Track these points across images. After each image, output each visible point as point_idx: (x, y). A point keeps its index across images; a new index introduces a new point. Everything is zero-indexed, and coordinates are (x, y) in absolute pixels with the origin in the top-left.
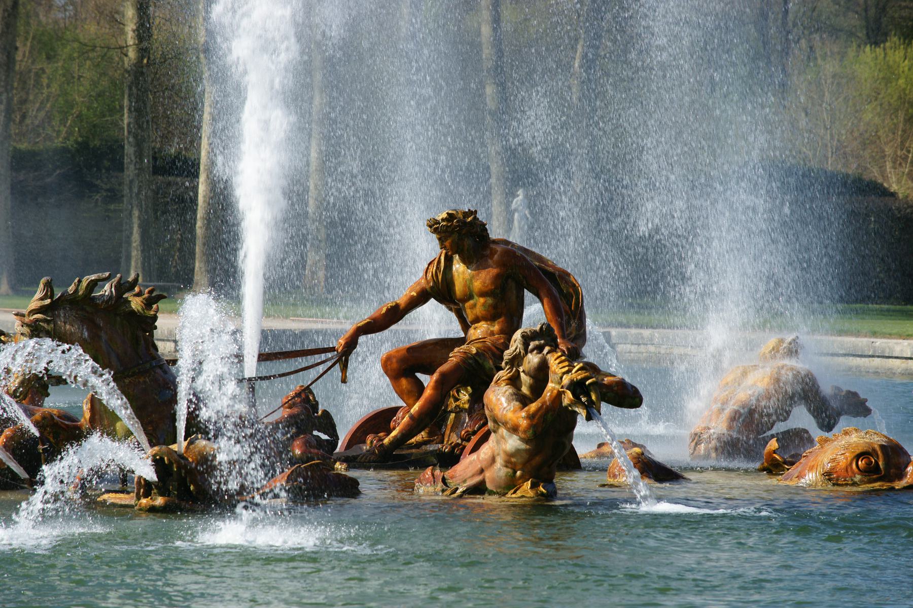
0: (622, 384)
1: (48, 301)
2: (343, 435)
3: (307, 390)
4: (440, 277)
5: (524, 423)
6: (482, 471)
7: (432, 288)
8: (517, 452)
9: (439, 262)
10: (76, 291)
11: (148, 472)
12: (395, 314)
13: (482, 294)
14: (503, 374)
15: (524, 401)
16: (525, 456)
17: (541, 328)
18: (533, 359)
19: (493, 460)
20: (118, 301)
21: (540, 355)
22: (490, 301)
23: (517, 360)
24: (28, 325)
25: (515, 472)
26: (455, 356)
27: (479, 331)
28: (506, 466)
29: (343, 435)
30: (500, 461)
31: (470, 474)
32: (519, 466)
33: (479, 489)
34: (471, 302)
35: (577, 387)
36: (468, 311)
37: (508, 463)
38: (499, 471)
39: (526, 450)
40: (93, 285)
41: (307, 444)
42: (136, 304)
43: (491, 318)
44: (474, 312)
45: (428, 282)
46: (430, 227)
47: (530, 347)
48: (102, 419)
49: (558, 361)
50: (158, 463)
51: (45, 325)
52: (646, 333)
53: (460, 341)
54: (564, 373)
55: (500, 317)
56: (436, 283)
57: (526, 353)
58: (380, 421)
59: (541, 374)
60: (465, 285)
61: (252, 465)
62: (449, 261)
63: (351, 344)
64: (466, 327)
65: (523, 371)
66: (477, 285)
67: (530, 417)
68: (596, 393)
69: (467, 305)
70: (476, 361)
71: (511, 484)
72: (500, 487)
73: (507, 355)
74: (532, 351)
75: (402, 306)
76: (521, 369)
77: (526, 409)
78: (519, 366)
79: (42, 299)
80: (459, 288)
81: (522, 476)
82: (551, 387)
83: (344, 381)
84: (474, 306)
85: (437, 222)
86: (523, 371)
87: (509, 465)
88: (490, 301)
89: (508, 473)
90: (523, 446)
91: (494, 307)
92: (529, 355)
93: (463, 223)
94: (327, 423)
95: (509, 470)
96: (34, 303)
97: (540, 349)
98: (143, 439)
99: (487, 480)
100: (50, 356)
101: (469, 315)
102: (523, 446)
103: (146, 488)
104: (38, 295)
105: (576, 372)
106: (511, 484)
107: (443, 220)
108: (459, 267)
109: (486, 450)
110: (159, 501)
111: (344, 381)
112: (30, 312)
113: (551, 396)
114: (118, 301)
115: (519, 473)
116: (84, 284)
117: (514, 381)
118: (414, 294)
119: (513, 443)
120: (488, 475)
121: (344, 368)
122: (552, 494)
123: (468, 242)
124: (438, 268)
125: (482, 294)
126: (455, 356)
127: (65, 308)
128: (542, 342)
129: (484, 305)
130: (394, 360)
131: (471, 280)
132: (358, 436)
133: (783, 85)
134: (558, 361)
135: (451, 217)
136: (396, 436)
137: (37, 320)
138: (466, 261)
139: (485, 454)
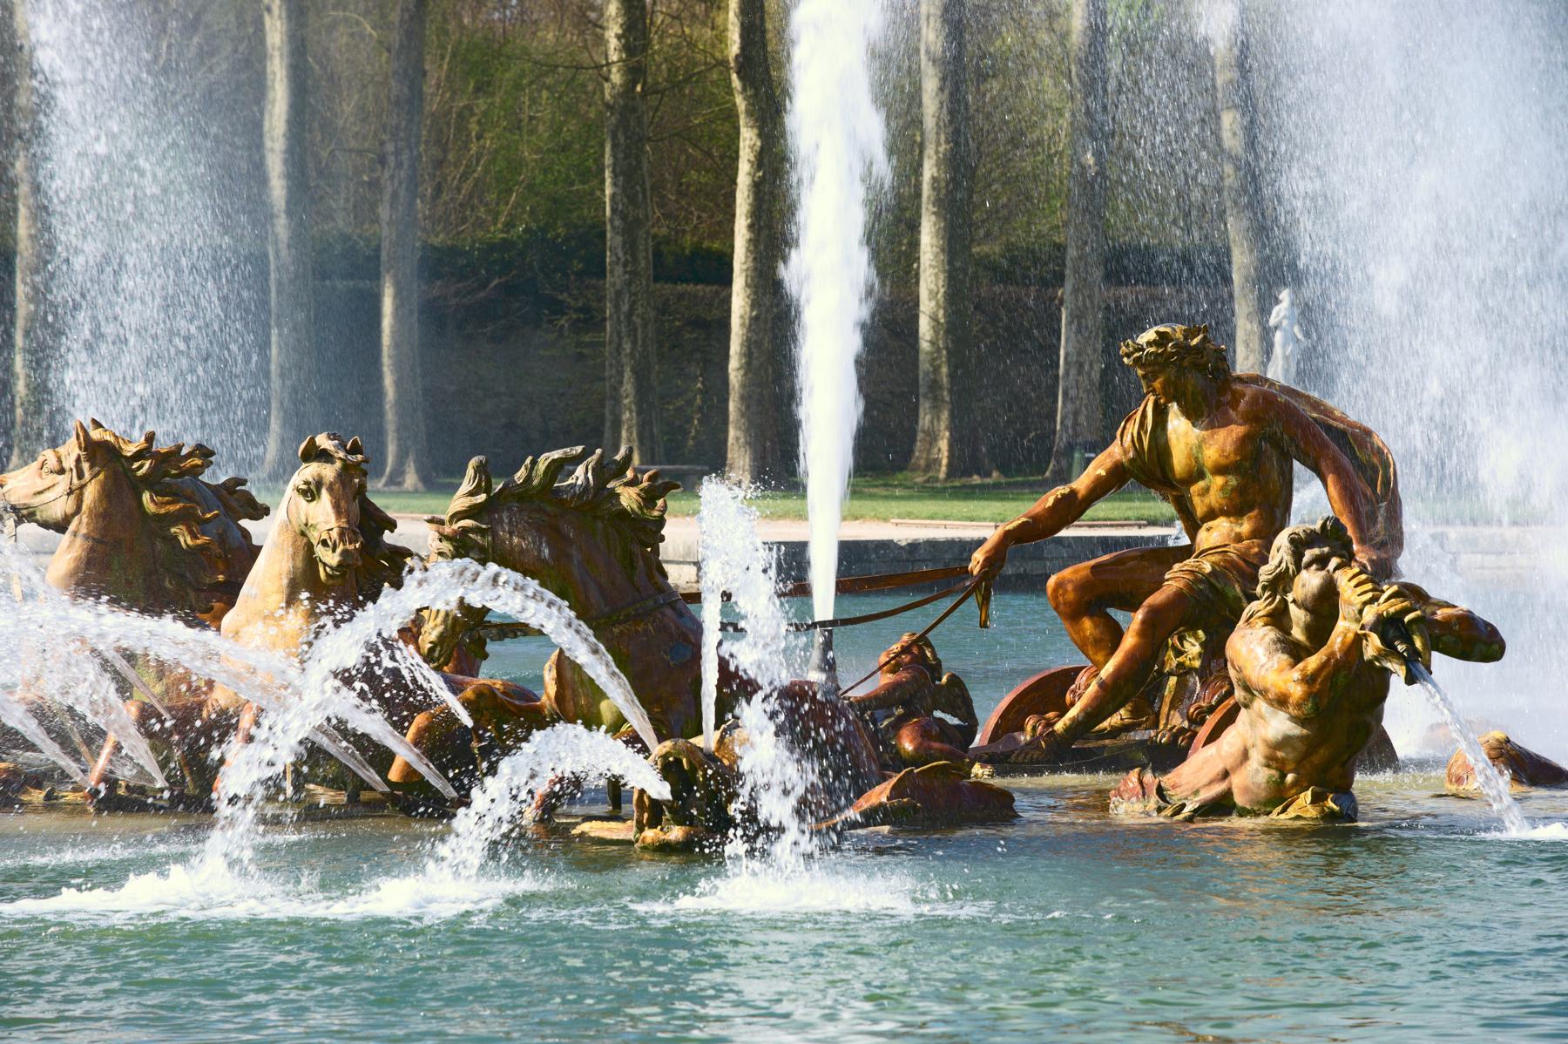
0: (1468, 620)
1: (482, 497)
2: (989, 710)
3: (922, 641)
5: (1297, 691)
6: (1226, 775)
7: (1131, 461)
8: (1285, 742)
10: (529, 478)
11: (646, 779)
13: (1220, 470)
14: (1259, 607)
15: (1296, 653)
17: (1324, 526)
18: (1309, 581)
20: (599, 494)
21: (1323, 573)
22: (1233, 481)
23: (1281, 582)
25: (1283, 776)
26: (1175, 579)
27: (1216, 533)
28: (1268, 766)
29: (989, 710)
30: (1257, 757)
31: (1206, 780)
32: (1291, 766)
33: (1221, 806)
34: (1201, 484)
35: (1389, 627)
36: (1196, 500)
37: (1270, 761)
38: (1253, 777)
39: (1301, 738)
40: (557, 468)
41: (924, 734)
42: (628, 498)
43: (1235, 510)
44: (1207, 501)
45: (1125, 452)
47: (1305, 559)
48: (577, 701)
50: (669, 769)
51: (478, 539)
53: (1186, 552)
54: (1365, 604)
55: (1251, 509)
56: (1139, 452)
57: (1299, 570)
58: (1050, 691)
59: (1325, 605)
60: (1190, 456)
62: (1161, 414)
64: (1193, 528)
66: (1211, 455)
67: (1308, 680)
68: (1422, 636)
69: (1194, 489)
70: (1212, 586)
71: (1278, 796)
72: (1258, 803)
73: (1265, 573)
74: (1308, 566)
76: (1290, 598)
77: (1300, 665)
78: (1286, 592)
79: (471, 494)
80: (1179, 461)
81: (1295, 784)
82: (1344, 628)
84: (1207, 490)
86: (1294, 601)
87: (1274, 764)
88: (1233, 481)
89: (1271, 777)
91: (1240, 490)
92: (1304, 572)
94: (958, 697)
95: (1273, 772)
96: (459, 502)
98: (638, 720)
99: (1235, 791)
100: (508, 595)
103: (654, 812)
104: (466, 486)
106: (1278, 796)
107: (1149, 344)
108: (1179, 427)
109: (1232, 739)
110: (676, 833)
112: (453, 517)
113: (1343, 643)
114: (599, 494)
115: (1290, 778)
116: (542, 466)
117: (1278, 619)
119: (1280, 725)
120: (1236, 781)
122: (1349, 812)
123: (1193, 381)
125: (1220, 470)
126: (1175, 579)
127: (510, 509)
128: (1326, 549)
129: (1222, 489)
131: (1200, 447)
132: (1011, 721)
134: (1355, 582)
137: (465, 530)
138: (1192, 414)
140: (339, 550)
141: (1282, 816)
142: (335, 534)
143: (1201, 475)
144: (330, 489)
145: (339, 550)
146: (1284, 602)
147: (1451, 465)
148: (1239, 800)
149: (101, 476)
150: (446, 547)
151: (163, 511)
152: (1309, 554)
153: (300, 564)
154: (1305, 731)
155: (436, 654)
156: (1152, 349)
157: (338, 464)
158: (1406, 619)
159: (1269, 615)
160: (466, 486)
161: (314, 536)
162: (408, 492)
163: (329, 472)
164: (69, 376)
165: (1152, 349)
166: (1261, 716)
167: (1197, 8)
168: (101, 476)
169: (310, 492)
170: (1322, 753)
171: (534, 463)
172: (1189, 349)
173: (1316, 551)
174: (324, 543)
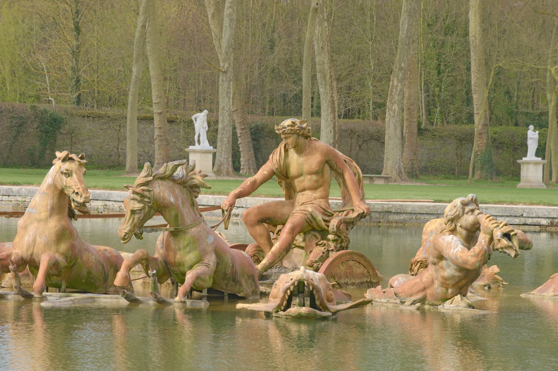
6: (424, 289)
7: (277, 169)
8: (453, 277)
16: (457, 280)
24: (137, 193)
25: (447, 290)
28: (442, 286)
30: (437, 284)
31: (416, 291)
39: (458, 277)
52: (15, 188)
54: (495, 227)
56: (280, 166)
57: (463, 215)
61: (501, 292)
65: (461, 226)
74: (467, 213)
75: (258, 181)
79: (146, 177)
80: (293, 170)
81: (452, 293)
82: (482, 238)
83: (226, 229)
85: (285, 128)
86: (461, 226)
87: (445, 286)
90: (457, 274)
92: (465, 216)
97: (472, 211)
99: (428, 295)
102: (457, 274)
105: (502, 227)
107: (288, 126)
108: (293, 155)
112: (138, 185)
113: (485, 241)
115: (450, 291)
120: (428, 291)
129: (310, 180)
130: (252, 215)
133: (293, 18)
134: (488, 220)
136: (265, 264)
137: (143, 190)
142: (81, 190)
143: (301, 175)
144: (76, 173)
146: (456, 225)
147: (65, 171)
150: (137, 197)
152: (467, 209)
153: (55, 201)
154: (460, 274)
155: (126, 237)
156: (290, 128)
158: (512, 234)
160: (143, 173)
161: (69, 192)
162: (532, 190)
164: (399, 142)
165: (290, 128)
166: (442, 268)
169: (68, 174)
170: (464, 282)
172: (302, 128)
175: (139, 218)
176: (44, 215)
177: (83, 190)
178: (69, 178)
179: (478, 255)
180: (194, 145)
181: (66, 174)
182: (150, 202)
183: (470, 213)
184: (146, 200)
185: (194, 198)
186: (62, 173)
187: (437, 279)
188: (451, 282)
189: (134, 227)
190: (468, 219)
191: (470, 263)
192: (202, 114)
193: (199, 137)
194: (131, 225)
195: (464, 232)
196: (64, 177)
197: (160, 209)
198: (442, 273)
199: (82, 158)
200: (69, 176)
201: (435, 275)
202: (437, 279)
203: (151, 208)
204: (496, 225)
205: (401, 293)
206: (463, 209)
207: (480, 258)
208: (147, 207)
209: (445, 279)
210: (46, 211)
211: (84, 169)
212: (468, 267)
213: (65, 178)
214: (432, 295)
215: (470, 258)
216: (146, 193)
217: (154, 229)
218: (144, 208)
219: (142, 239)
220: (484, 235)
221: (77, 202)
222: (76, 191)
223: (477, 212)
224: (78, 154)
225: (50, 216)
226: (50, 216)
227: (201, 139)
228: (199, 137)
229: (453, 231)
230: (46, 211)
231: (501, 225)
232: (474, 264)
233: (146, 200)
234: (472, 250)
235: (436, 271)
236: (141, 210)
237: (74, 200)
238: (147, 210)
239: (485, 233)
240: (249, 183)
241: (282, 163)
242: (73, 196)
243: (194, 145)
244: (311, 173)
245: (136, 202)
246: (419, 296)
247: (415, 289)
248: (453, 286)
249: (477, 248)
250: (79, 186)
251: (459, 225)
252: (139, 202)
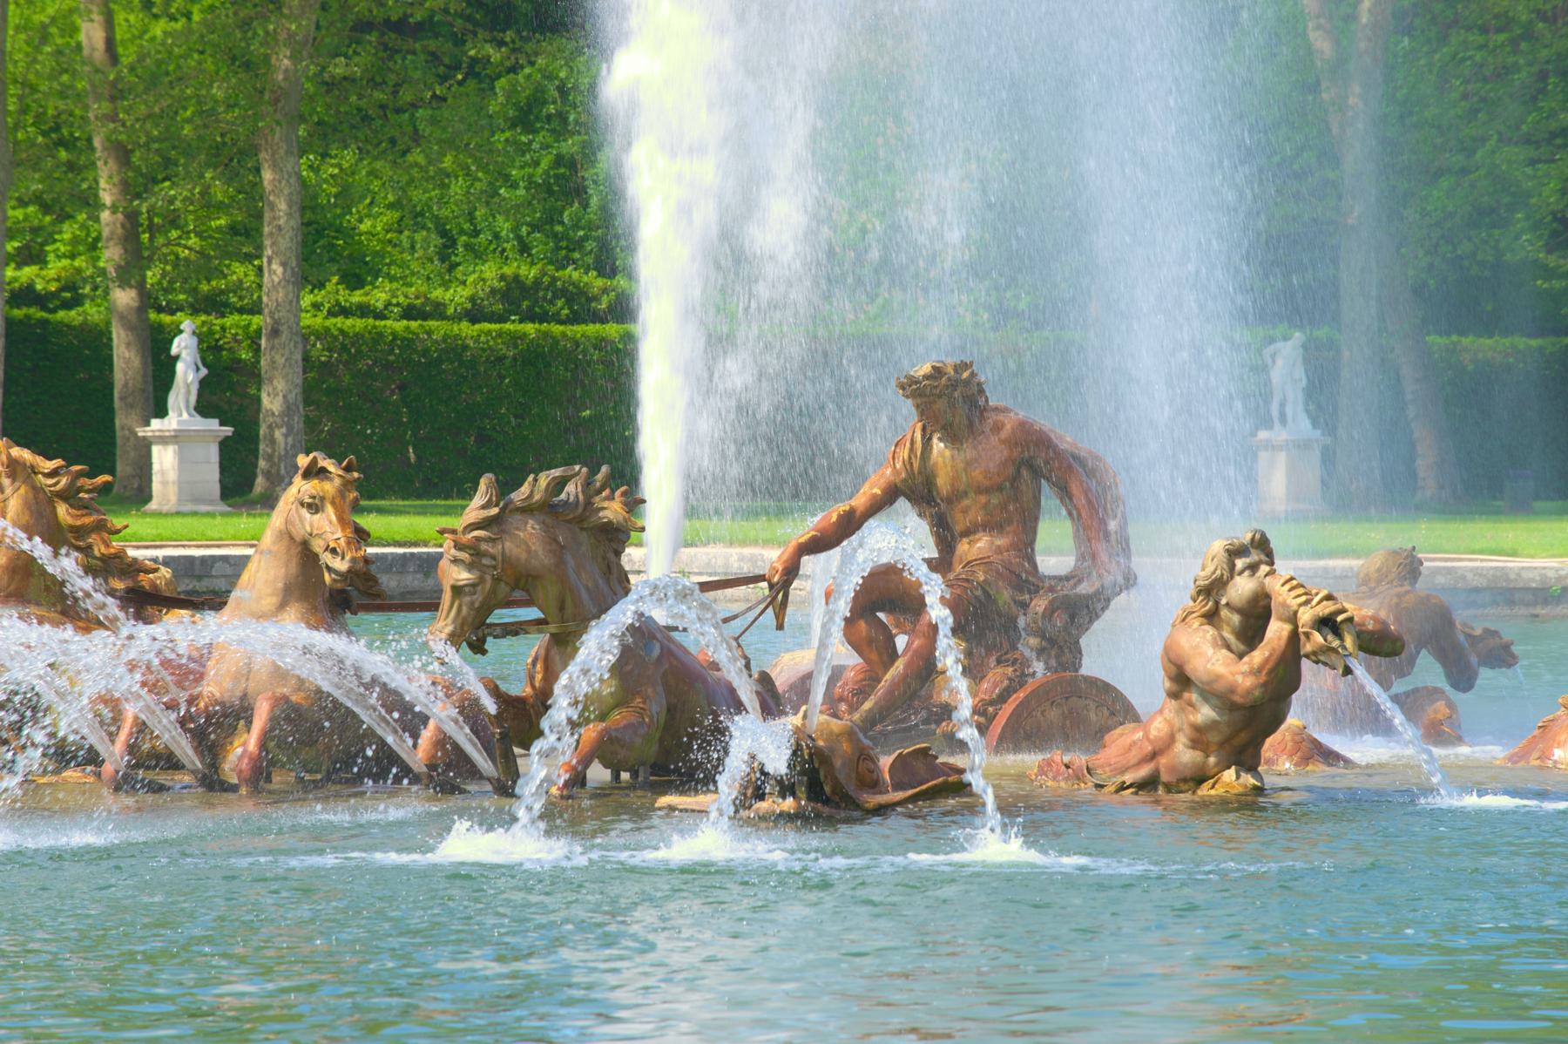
1: (495, 511)
4: (916, 465)
6: (1154, 755)
7: (905, 481)
8: (1212, 726)
9: (913, 442)
10: (531, 495)
12: (849, 524)
16: (1226, 731)
19: (1171, 739)
31: (1135, 760)
36: (959, 516)
46: (903, 388)
49: (1287, 587)
54: (1300, 605)
56: (911, 474)
62: (927, 442)
63: (791, 571)
79: (483, 507)
80: (943, 482)
81: (1217, 764)
82: (1277, 630)
83: (780, 627)
86: (1227, 604)
92: (1238, 579)
93: (954, 384)
97: (1253, 568)
99: (1162, 770)
101: (960, 522)
107: (926, 377)
108: (938, 446)
111: (780, 627)
118: (877, 491)
120: (1163, 761)
121: (781, 609)
124: (912, 449)
134: (1287, 587)
135: (938, 372)
136: (871, 710)
137: (478, 539)
139: (1159, 730)
140: (348, 558)
141: (1213, 792)
142: (342, 542)
144: (333, 503)
145: (348, 558)
146: (1217, 603)
147: (307, 500)
148: (1164, 777)
149: (22, 491)
151: (79, 523)
153: (294, 568)
157: (337, 481)
158: (1340, 618)
159: (1203, 616)
160: (479, 499)
161: (317, 546)
163: (329, 488)
166: (1191, 705)
167: (589, 5)
168: (22, 491)
169: (314, 507)
170: (1244, 736)
171: (535, 480)
173: (1248, 560)
174: (334, 551)
175: (472, 603)
176: (270, 602)
177: (349, 543)
178: (317, 517)
179: (1260, 670)
180: (1271, 428)
181: (309, 506)
182: (495, 568)
183: (1247, 573)
184: (485, 561)
185: (611, 556)
186: (302, 504)
187: (1180, 730)
188: (1214, 738)
189: (462, 625)
190: (1242, 587)
191: (1239, 690)
192: (1290, 343)
193: (1282, 405)
194: (454, 621)
195: (1236, 619)
196: (304, 512)
197: (522, 582)
198: (1191, 717)
199: (348, 469)
200: (317, 512)
201: (1177, 723)
202: (1180, 730)
203: (496, 580)
204: (1303, 598)
205: (1102, 767)
206: (1232, 567)
207: (1263, 678)
208: (488, 578)
209: (1198, 729)
210: (272, 595)
211: (353, 495)
212: (1237, 699)
213: (308, 516)
214: (1172, 769)
215: (1240, 679)
216: (484, 546)
217: (513, 630)
218: (481, 580)
219: (484, 652)
220: (1279, 624)
221: (336, 572)
222: (332, 545)
223: (1264, 569)
224: (338, 457)
225: (282, 606)
226: (282, 606)
227: (1289, 410)
228: (1282, 405)
229: (1211, 617)
230: (272, 595)
231: (1317, 599)
232: (1249, 692)
233: (485, 561)
234: (1246, 659)
235: (1181, 710)
236: (473, 585)
237: (328, 568)
238: (488, 585)
239: (1280, 619)
240: (834, 519)
241: (916, 465)
242: (327, 558)
243: (1271, 428)
244: (980, 490)
245: (461, 568)
246: (1143, 772)
247: (1135, 756)
248: (1221, 745)
249: (1258, 656)
250: (339, 534)
251: (1223, 601)
252: (470, 567)
